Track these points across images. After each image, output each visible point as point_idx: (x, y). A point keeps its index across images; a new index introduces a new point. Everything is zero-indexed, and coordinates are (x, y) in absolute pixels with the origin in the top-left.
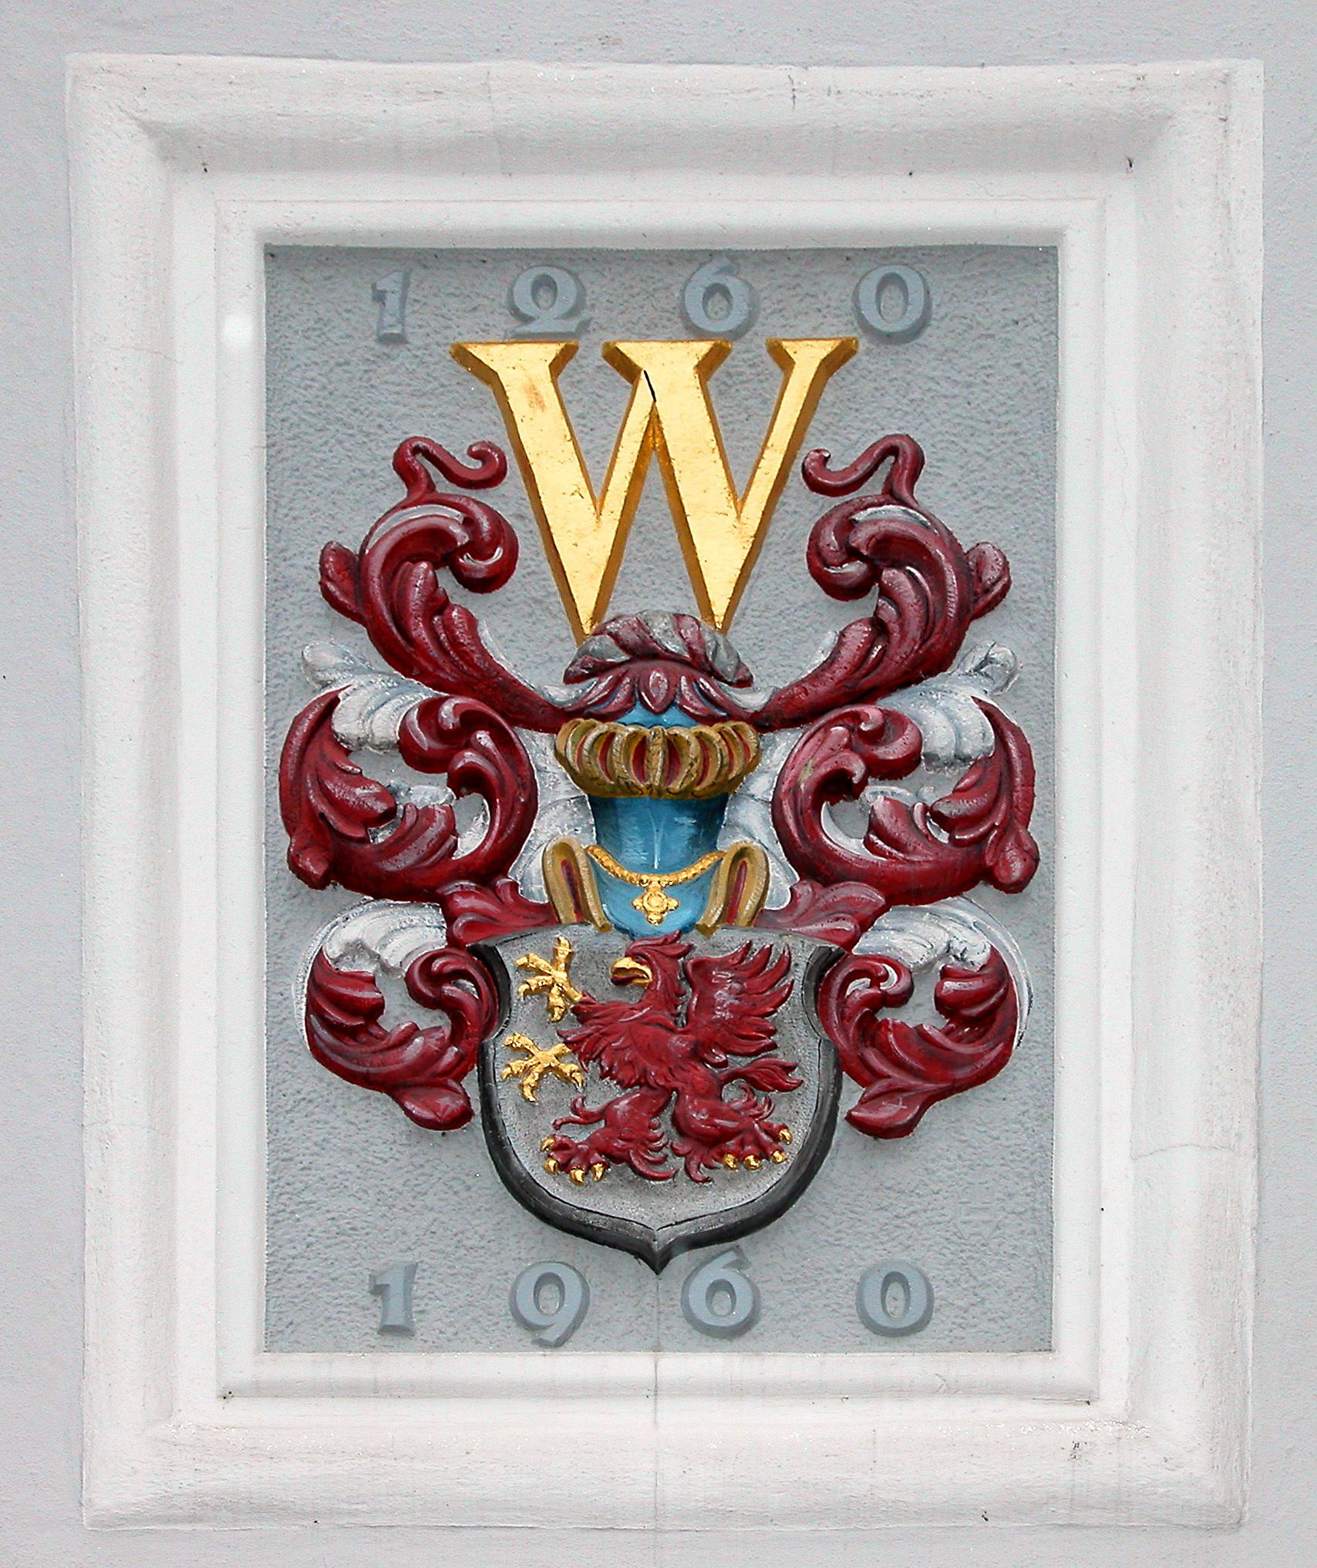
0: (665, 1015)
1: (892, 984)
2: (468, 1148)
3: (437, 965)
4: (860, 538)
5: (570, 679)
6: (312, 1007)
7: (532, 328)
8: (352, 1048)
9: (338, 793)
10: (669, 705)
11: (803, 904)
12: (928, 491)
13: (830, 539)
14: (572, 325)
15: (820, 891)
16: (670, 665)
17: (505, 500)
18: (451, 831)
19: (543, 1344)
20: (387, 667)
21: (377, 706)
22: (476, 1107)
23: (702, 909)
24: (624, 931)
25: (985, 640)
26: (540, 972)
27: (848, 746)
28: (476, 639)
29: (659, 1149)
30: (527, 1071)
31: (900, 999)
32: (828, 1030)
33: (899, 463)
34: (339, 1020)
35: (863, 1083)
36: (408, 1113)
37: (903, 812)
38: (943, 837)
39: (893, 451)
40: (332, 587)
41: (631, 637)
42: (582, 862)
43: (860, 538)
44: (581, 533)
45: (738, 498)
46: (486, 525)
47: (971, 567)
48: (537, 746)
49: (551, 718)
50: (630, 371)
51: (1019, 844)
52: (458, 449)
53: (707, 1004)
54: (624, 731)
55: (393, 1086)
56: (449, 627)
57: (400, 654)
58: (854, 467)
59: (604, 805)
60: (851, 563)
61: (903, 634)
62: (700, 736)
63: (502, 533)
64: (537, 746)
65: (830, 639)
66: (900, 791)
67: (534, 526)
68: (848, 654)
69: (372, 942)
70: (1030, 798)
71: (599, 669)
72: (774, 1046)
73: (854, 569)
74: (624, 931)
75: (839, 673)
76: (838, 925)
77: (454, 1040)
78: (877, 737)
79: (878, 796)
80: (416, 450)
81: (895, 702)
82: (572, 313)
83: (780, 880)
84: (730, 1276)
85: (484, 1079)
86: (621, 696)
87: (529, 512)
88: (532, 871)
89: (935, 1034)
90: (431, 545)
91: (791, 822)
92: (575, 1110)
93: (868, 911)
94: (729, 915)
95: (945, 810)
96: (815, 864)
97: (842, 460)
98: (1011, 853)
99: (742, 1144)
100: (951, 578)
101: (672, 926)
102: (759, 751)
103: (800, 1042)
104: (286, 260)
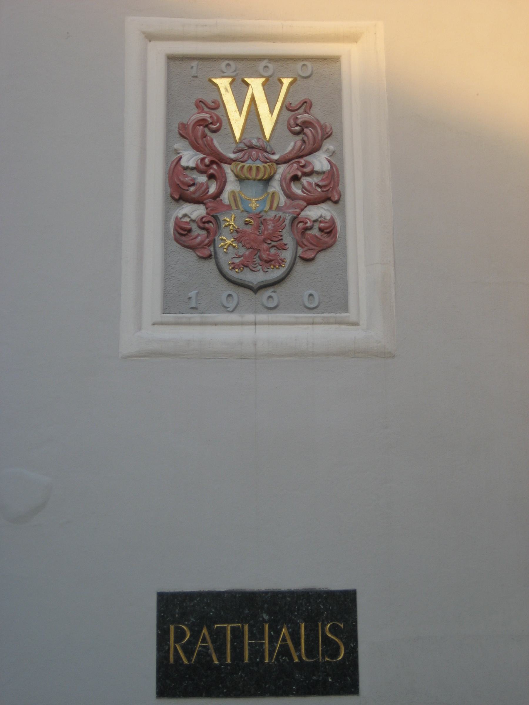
0: (256, 232)
1: (309, 224)
2: (211, 265)
3: (204, 220)
4: (299, 122)
5: (235, 153)
6: (175, 229)
7: (225, 74)
8: (183, 238)
9: (182, 179)
10: (257, 159)
11: (288, 204)
12: (313, 111)
13: (292, 122)
14: (234, 74)
15: (292, 202)
16: (257, 150)
17: (219, 112)
18: (208, 188)
19: (229, 312)
20: (193, 150)
21: (190, 158)
22: (213, 253)
23: (265, 206)
24: (247, 212)
25: (329, 145)
26: (228, 222)
27: (297, 169)
28: (213, 144)
29: (255, 264)
30: (225, 245)
31: (311, 228)
32: (294, 235)
33: (306, 105)
34: (182, 233)
35: (303, 248)
36: (197, 254)
37: (310, 184)
38: (319, 190)
39: (306, 102)
40: (181, 132)
41: (248, 144)
42: (237, 195)
43: (299, 122)
44: (237, 122)
45: (272, 112)
46: (215, 118)
47: (323, 128)
48: (227, 168)
49: (229, 161)
50: (248, 85)
51: (336, 191)
52: (209, 101)
53: (266, 229)
54: (247, 165)
55: (193, 248)
56: (207, 141)
57: (196, 147)
58: (297, 106)
59: (240, 179)
60: (299, 128)
61: (309, 143)
62: (264, 166)
63: (219, 120)
64: (227, 168)
65: (292, 144)
66: (309, 179)
67: (226, 118)
68: (297, 147)
69: (189, 214)
70: (338, 181)
71: (241, 151)
72: (282, 239)
73: (298, 128)
74: (247, 212)
75: (295, 152)
76: (296, 210)
77: (208, 237)
78: (303, 167)
79: (305, 180)
80: (200, 101)
81: (308, 158)
82: (235, 71)
83: (283, 199)
84: (273, 294)
85: (214, 247)
86: (246, 157)
87: (225, 115)
88: (225, 197)
89: (319, 236)
90: (202, 122)
91: (284, 186)
92: (236, 255)
93: (303, 207)
94: (271, 208)
95: (320, 184)
96: (290, 196)
97: (295, 103)
98: (335, 193)
99: (275, 263)
100: (319, 131)
101: (258, 211)
102: (277, 169)
103: (288, 239)
104: (171, 59)
